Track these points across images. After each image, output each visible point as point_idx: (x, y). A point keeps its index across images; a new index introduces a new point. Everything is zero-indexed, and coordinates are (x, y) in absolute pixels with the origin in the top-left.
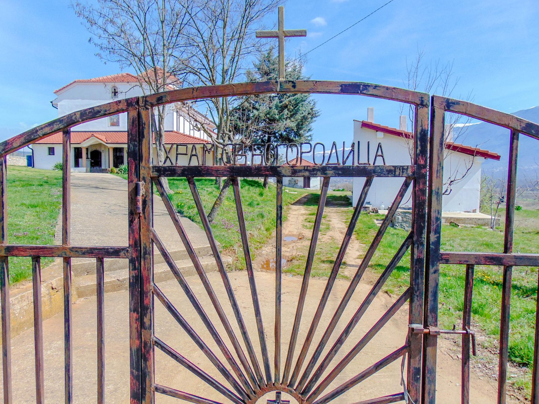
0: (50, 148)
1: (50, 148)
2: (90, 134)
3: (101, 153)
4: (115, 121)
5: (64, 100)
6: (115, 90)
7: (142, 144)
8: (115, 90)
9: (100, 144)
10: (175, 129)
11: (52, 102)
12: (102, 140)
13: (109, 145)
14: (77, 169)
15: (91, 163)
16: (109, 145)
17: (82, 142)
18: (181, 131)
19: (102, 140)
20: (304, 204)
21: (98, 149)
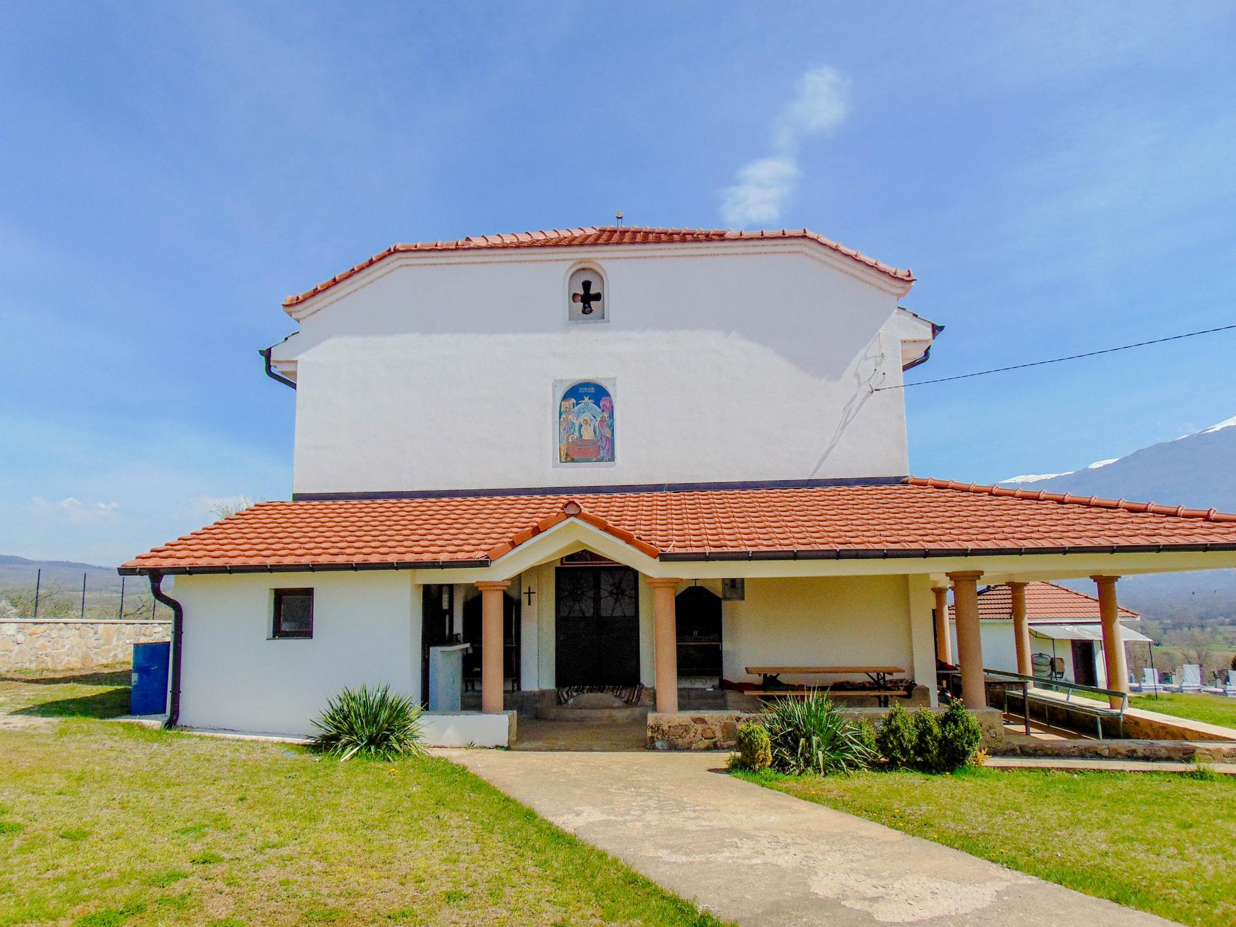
6: (587, 285)
8: (587, 285)
14: (472, 720)
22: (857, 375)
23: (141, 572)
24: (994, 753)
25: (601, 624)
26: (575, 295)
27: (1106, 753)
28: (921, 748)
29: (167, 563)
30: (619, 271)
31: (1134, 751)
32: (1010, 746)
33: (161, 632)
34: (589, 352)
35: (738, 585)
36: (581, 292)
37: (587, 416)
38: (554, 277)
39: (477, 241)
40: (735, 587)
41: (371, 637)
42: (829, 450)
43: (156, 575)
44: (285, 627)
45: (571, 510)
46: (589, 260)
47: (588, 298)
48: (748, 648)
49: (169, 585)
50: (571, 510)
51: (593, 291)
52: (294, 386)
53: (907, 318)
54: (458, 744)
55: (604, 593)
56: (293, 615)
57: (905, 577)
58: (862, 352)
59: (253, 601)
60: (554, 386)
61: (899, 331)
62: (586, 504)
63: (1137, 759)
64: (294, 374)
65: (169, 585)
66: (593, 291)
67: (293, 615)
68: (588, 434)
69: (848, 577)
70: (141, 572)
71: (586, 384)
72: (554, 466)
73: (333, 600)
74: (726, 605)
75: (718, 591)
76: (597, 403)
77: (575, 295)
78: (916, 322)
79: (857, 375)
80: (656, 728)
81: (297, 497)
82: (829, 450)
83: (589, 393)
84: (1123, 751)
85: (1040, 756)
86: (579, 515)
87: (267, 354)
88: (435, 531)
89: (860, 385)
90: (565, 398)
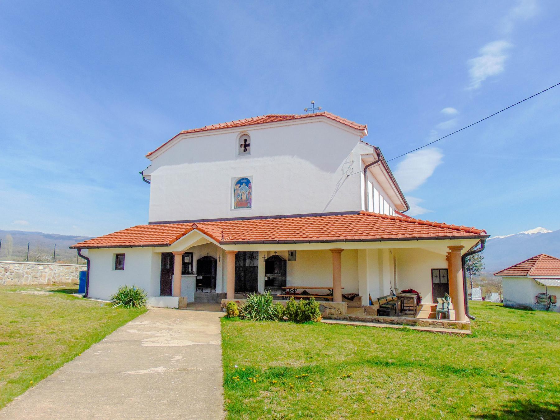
0: (117, 256)
1: (117, 256)
2: (189, 226)
3: (216, 261)
4: (244, 198)
5: (161, 168)
6: (245, 141)
7: (322, 300)
8: (245, 141)
9: (209, 245)
10: (363, 209)
11: (142, 173)
12: (211, 236)
13: (226, 248)
14: (166, 299)
15: (198, 281)
16: (226, 248)
17: (173, 241)
18: (371, 210)
19: (211, 236)
20: (357, 262)
21: (212, 254)
22: (342, 170)
23: (75, 248)
24: (324, 318)
25: (245, 269)
26: (241, 145)
27: (382, 321)
28: (296, 314)
29: (82, 245)
30: (256, 135)
31: (393, 321)
32: (346, 317)
33: (85, 269)
34: (244, 167)
35: (294, 253)
36: (243, 144)
37: (244, 191)
38: (232, 139)
39: (209, 127)
40: (292, 254)
41: (143, 270)
42: (330, 201)
43: (79, 249)
44: (119, 267)
45: (194, 227)
46: (244, 131)
47: (246, 145)
48: (297, 278)
49: (84, 252)
50: (194, 227)
51: (247, 143)
52: (150, 183)
53: (363, 145)
54: (163, 306)
55: (247, 258)
56: (119, 262)
57: (356, 251)
58: (345, 161)
59: (109, 257)
60: (232, 180)
61: (362, 151)
62: (200, 225)
63: (394, 324)
64: (150, 180)
65: (84, 252)
66: (247, 143)
67: (119, 262)
68: (244, 198)
69: (312, 251)
70: (75, 248)
71: (243, 179)
72: (231, 210)
73: (131, 256)
74: (288, 263)
75: (286, 256)
76: (247, 186)
77: (241, 145)
78: (367, 147)
79: (342, 170)
80: (224, 304)
81: (150, 223)
82: (330, 201)
83: (244, 182)
84: (389, 321)
85: (356, 321)
86: (197, 228)
87: (142, 173)
88: (332, 233)
89: (343, 174)
90: (236, 185)
